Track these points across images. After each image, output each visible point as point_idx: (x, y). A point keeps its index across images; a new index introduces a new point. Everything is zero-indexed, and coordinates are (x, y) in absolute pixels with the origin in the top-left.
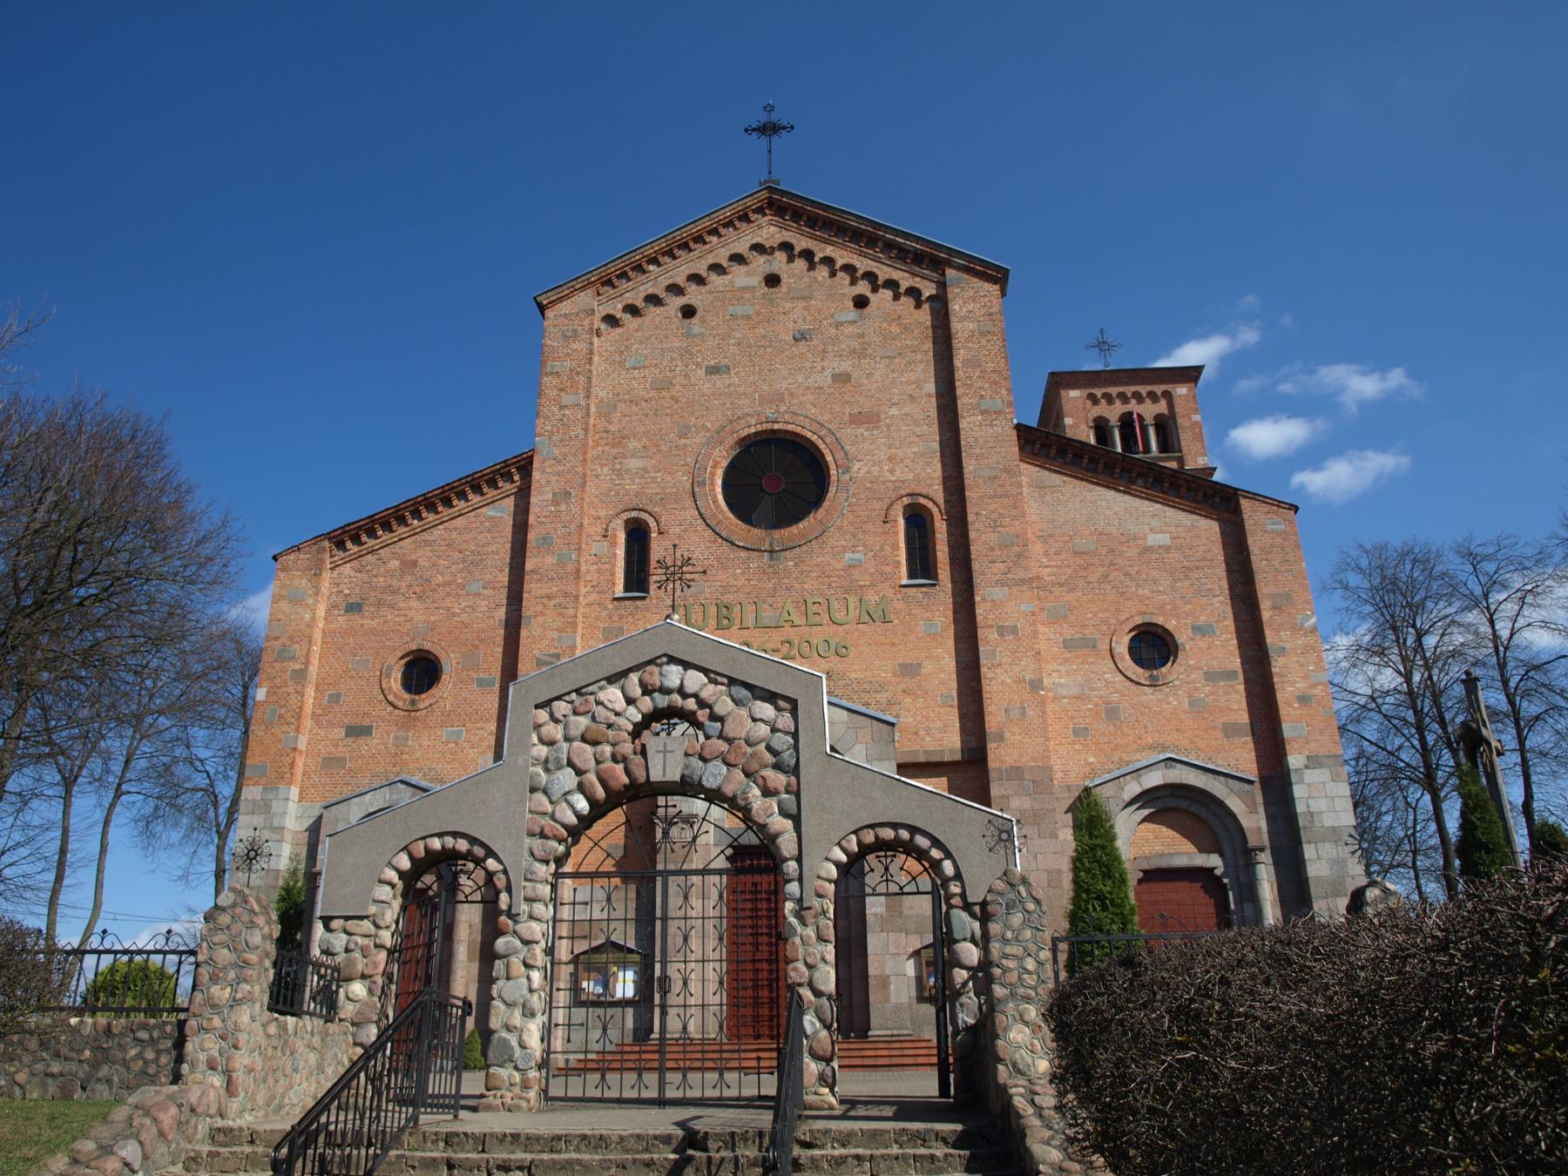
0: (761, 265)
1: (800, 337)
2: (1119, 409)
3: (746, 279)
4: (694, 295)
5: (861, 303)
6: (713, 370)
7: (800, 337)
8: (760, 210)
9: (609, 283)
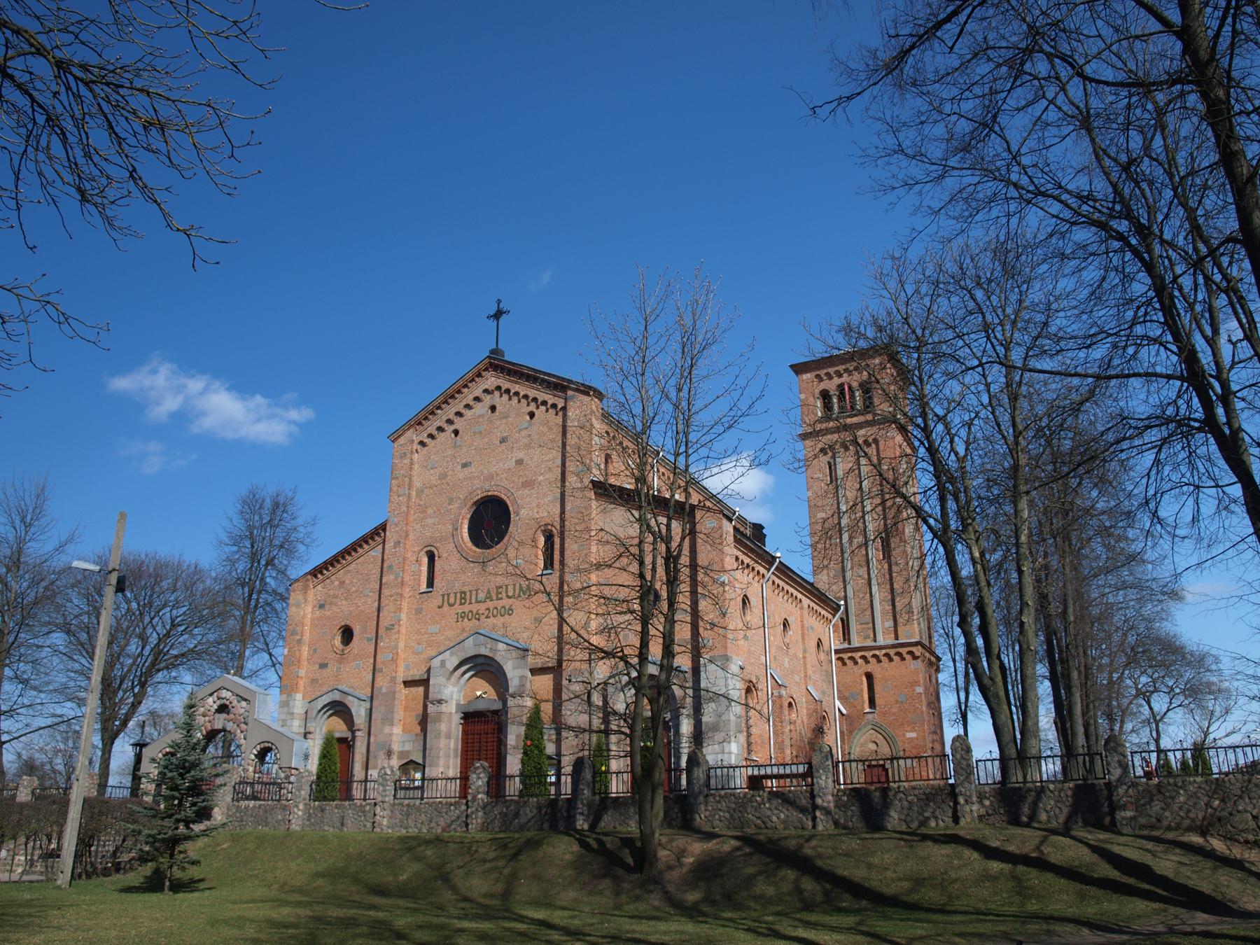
0: (488, 400)
1: (503, 440)
2: (837, 381)
3: (481, 409)
4: (459, 424)
5: (532, 415)
6: (465, 465)
7: (503, 440)
8: (486, 370)
9: (420, 423)
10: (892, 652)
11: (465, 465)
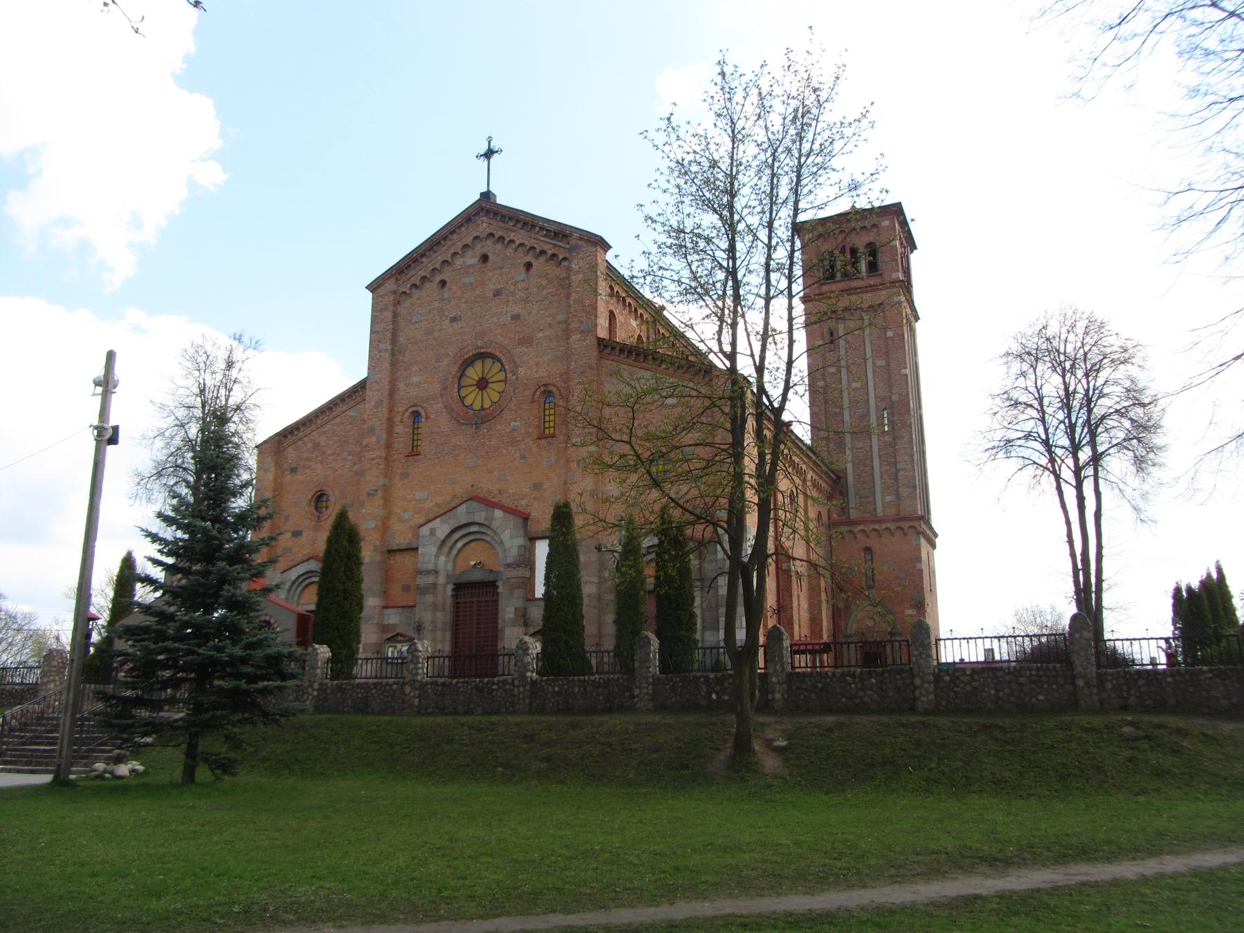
6: (453, 320)
10: (892, 526)
11: (453, 320)
